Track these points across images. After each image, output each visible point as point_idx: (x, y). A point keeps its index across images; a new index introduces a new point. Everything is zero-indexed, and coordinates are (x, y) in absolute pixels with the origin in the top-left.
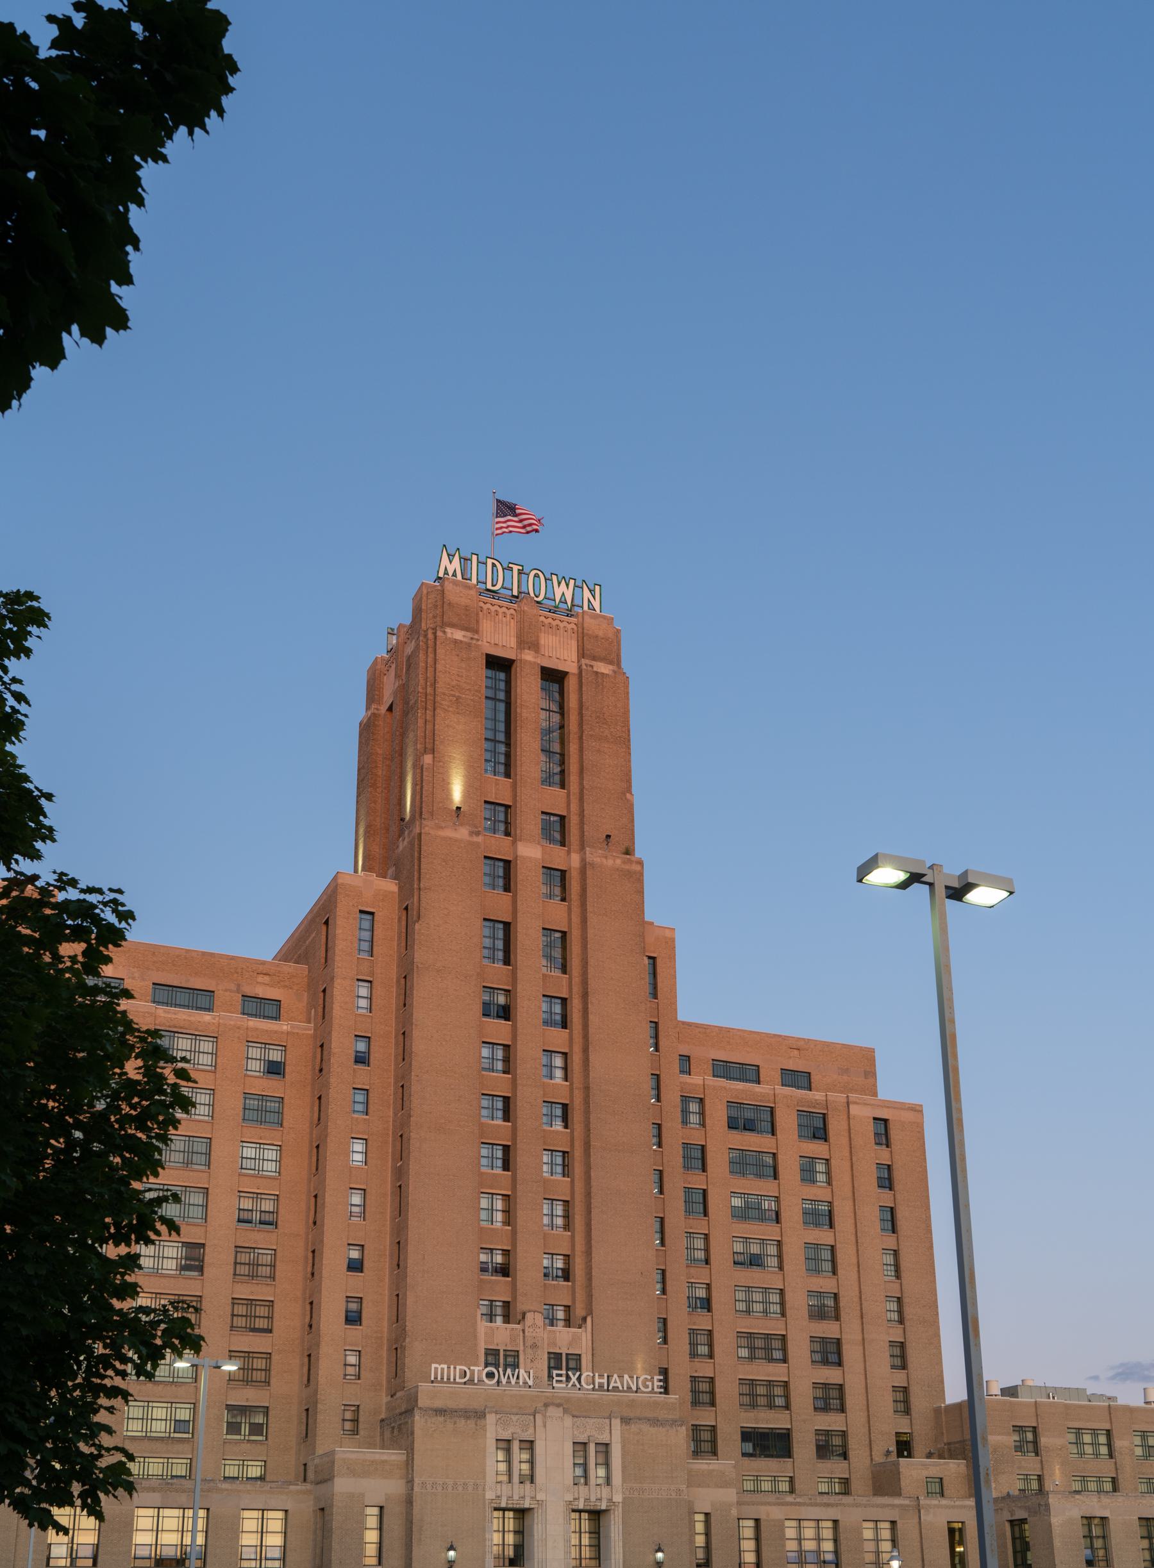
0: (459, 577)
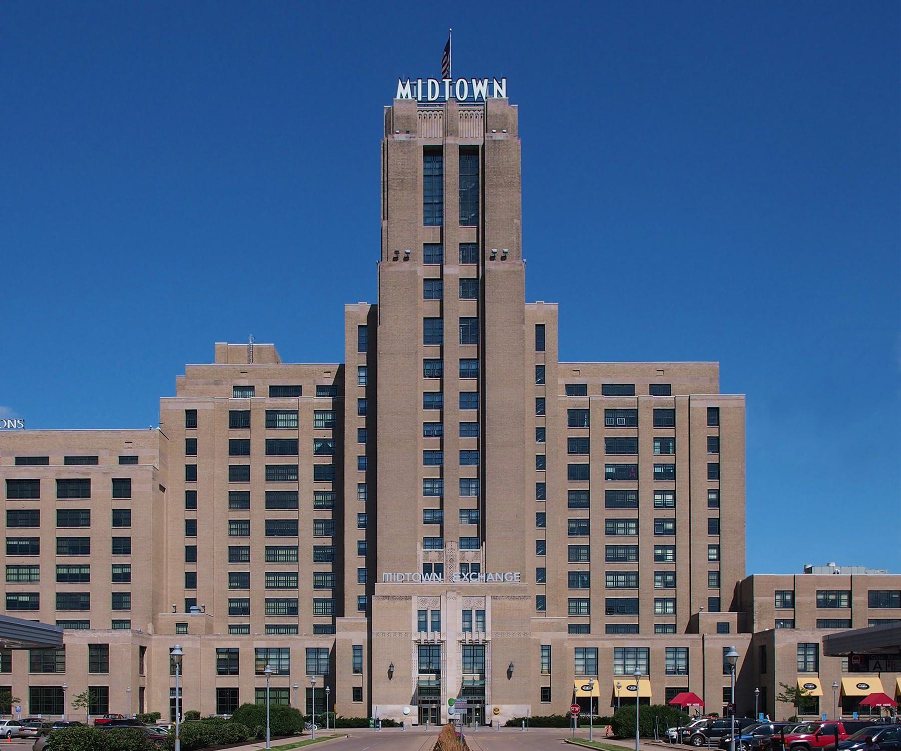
0: (410, 97)
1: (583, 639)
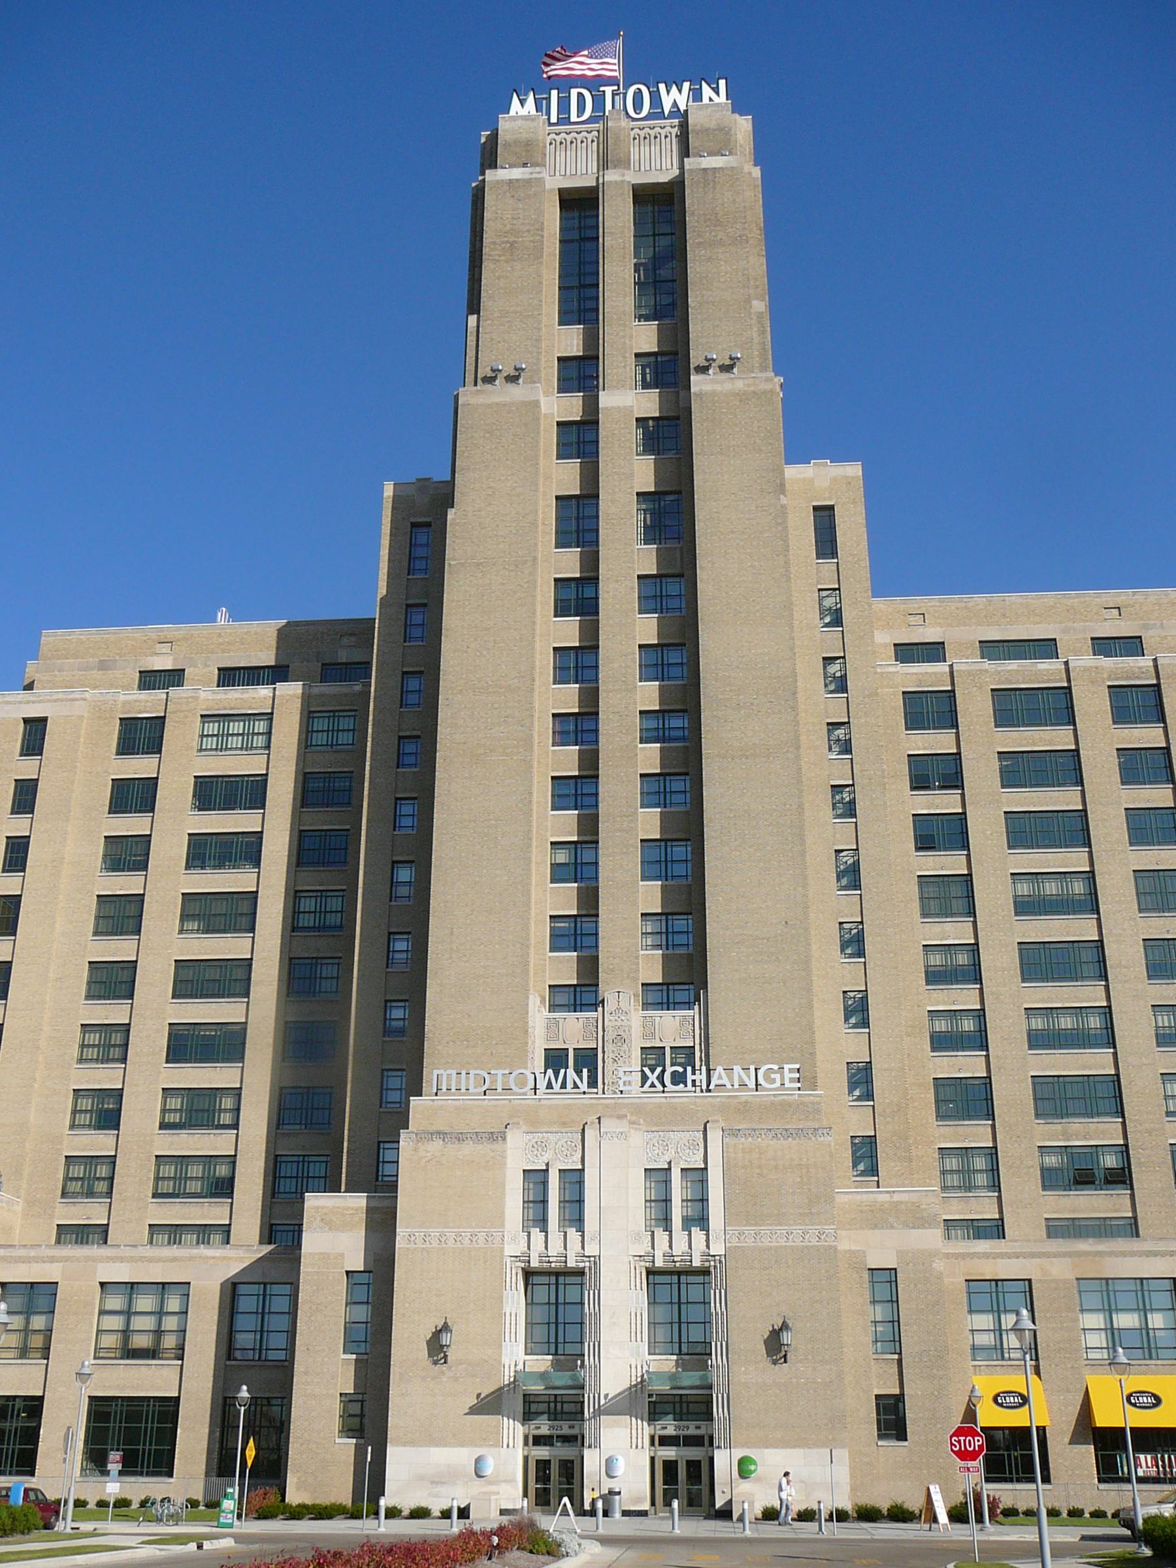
1: (986, 1255)
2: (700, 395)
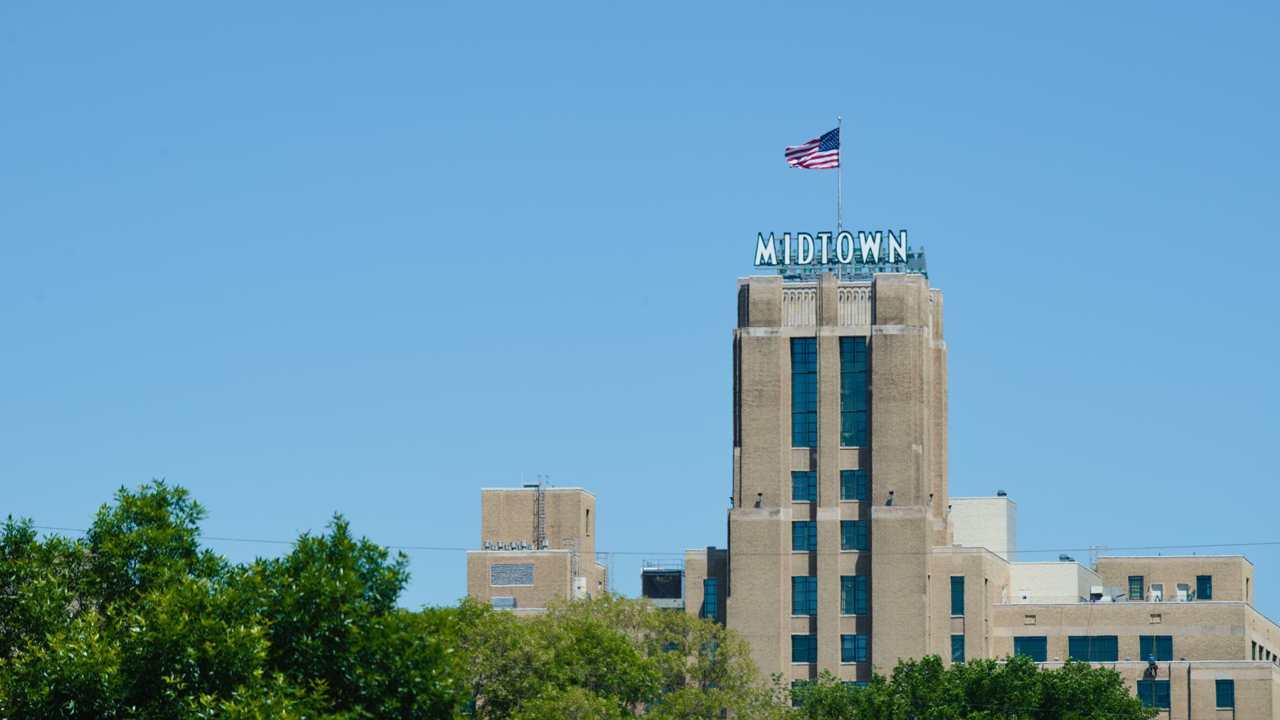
2: (877, 520)
